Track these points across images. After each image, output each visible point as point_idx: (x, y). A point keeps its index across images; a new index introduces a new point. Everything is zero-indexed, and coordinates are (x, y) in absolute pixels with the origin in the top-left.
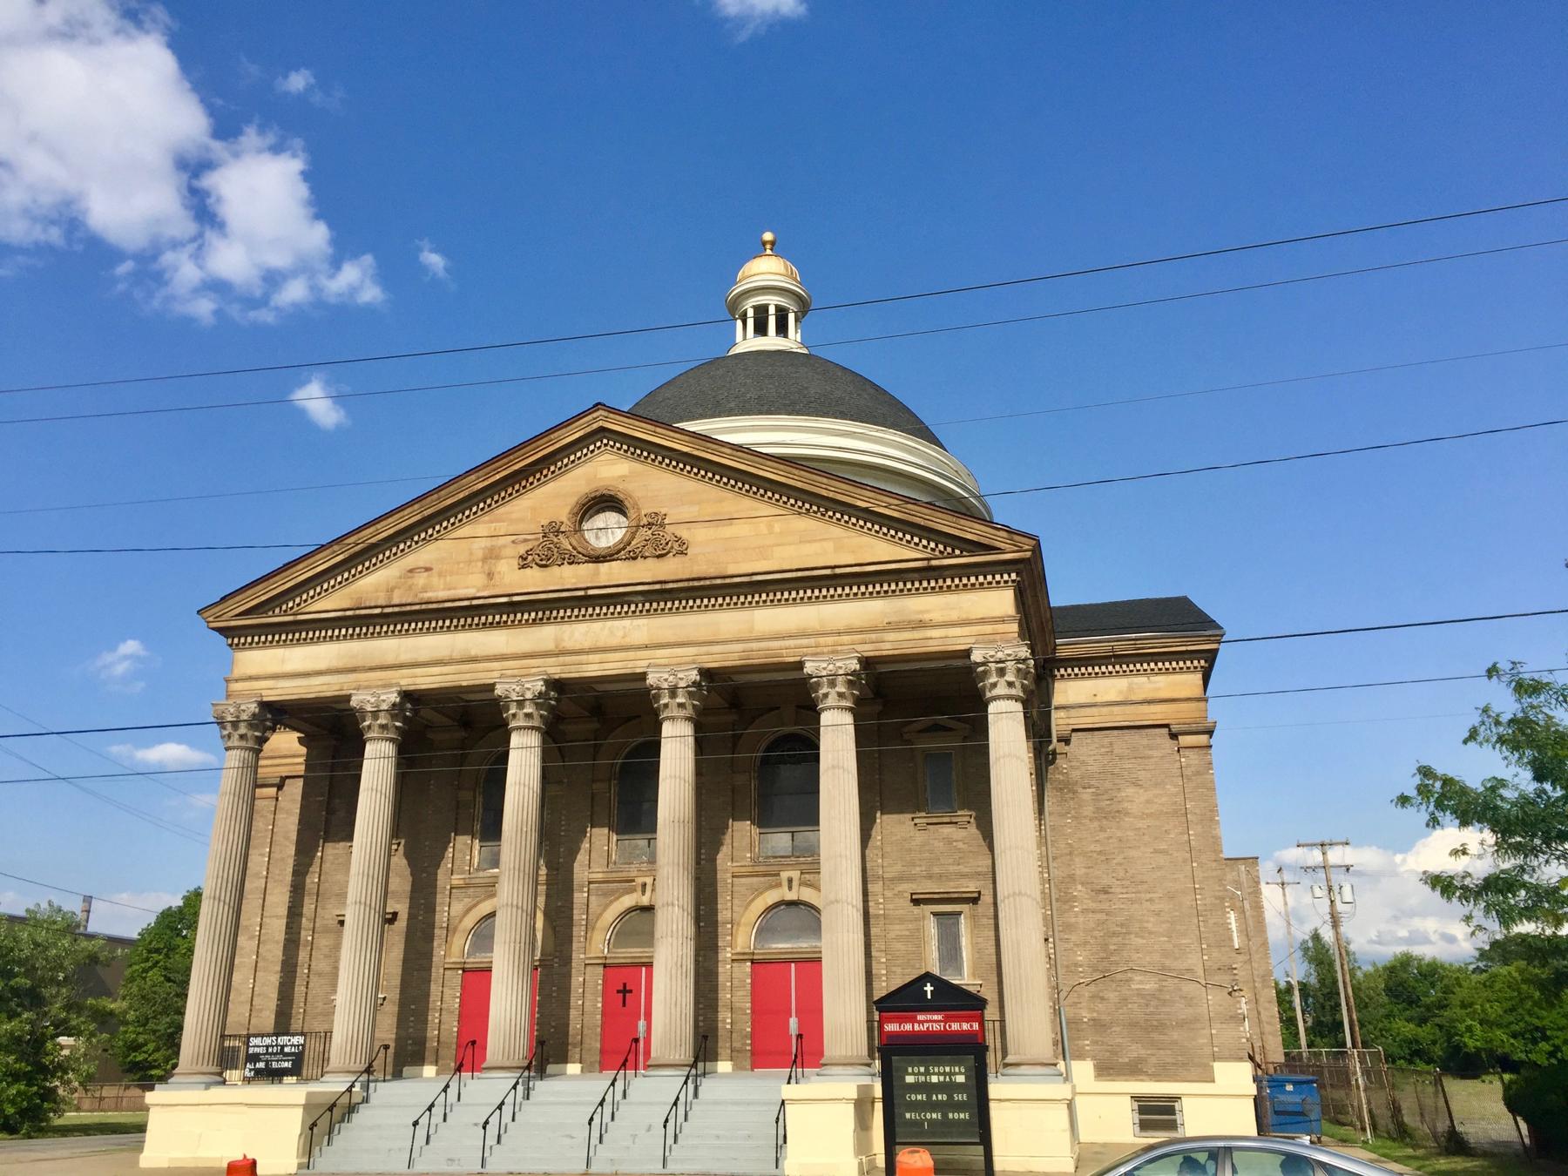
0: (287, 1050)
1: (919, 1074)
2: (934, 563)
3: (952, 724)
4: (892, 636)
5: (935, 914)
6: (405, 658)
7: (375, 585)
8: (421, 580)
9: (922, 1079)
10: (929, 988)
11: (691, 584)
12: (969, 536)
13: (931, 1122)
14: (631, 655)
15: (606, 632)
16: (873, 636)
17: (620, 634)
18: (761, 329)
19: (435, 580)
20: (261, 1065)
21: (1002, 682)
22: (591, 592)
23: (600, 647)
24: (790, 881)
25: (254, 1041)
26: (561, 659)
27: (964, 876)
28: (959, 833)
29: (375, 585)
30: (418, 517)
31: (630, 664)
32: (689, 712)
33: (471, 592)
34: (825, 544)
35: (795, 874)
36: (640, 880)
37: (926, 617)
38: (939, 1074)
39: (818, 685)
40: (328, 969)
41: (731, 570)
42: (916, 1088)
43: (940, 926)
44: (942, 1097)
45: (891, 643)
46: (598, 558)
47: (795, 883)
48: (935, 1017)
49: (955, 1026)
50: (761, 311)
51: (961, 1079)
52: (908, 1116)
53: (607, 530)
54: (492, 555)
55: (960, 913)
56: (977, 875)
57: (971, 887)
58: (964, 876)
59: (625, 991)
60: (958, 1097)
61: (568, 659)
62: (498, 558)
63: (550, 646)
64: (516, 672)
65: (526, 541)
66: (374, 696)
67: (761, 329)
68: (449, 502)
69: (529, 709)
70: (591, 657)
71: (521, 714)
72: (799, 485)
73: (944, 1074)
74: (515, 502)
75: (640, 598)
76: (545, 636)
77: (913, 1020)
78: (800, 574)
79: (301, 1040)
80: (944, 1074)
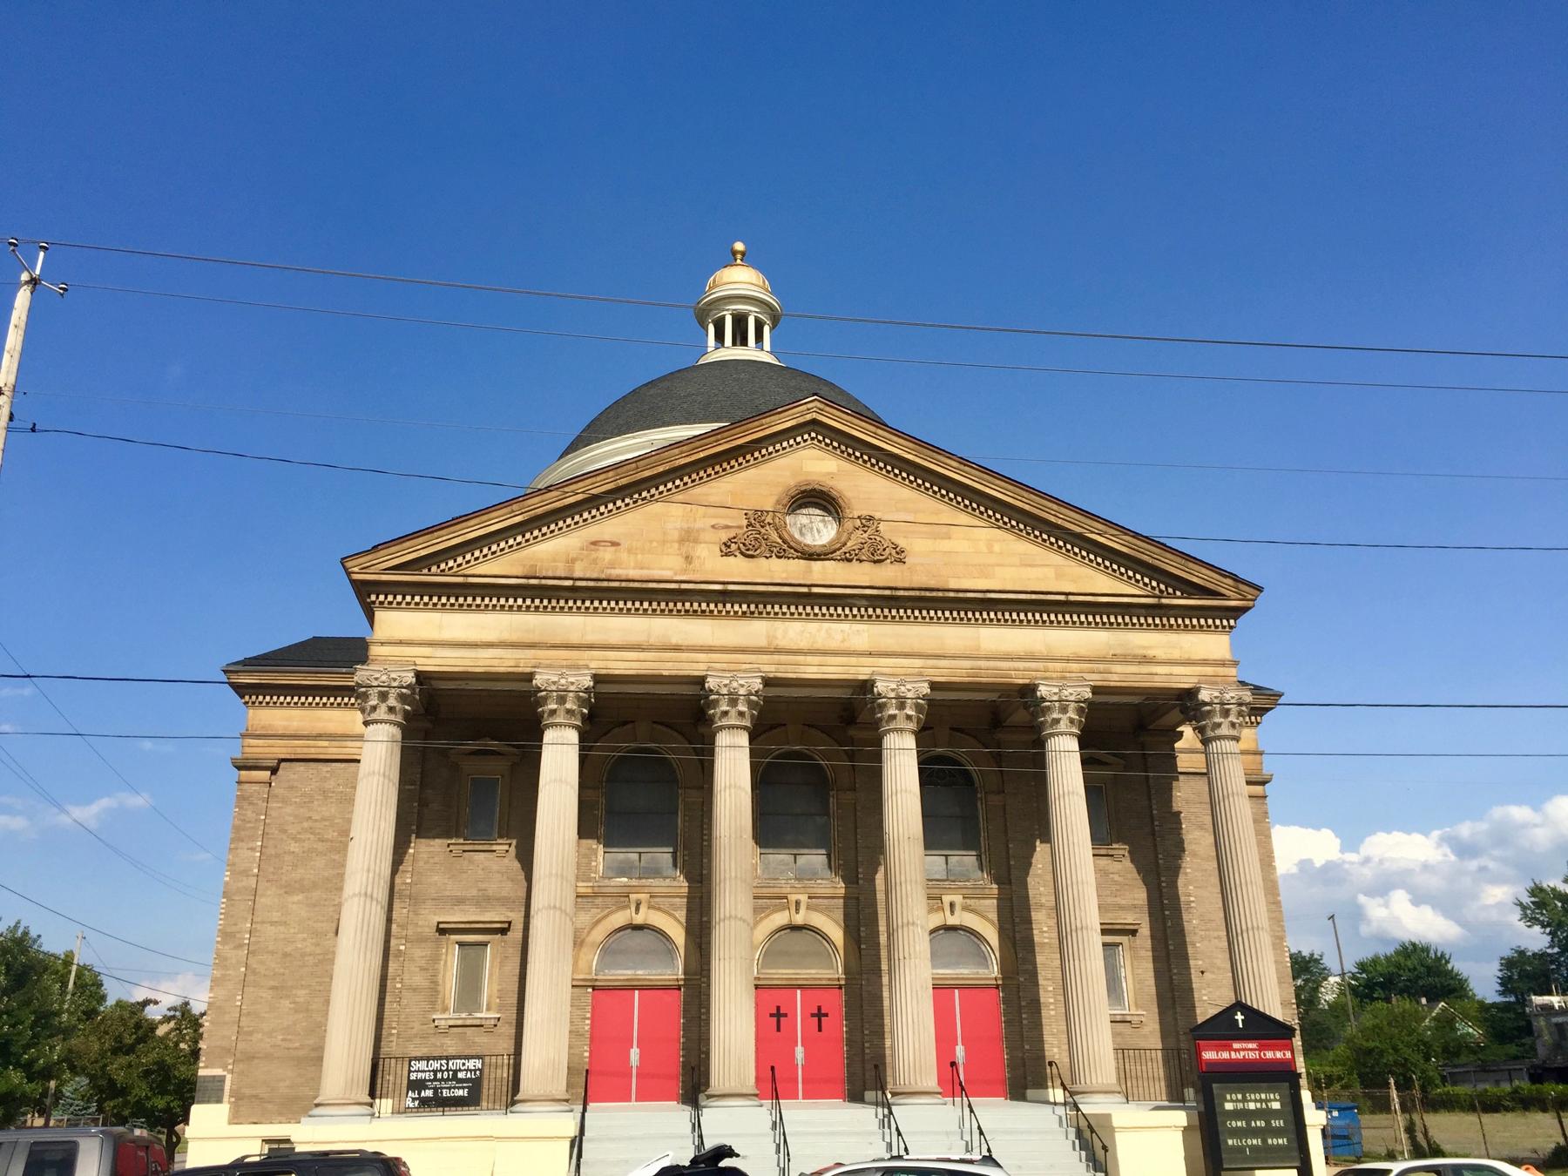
0: (460, 1075)
1: (1237, 1101)
2: (1164, 601)
3: (1111, 759)
4: (1118, 668)
5: (461, 944)
6: (614, 639)
7: (552, 553)
8: (607, 554)
9: (1240, 1106)
10: (1239, 1017)
11: (923, 593)
12: (1195, 580)
13: (1252, 1148)
14: (853, 660)
15: (823, 633)
16: (1101, 667)
17: (839, 637)
18: (720, 337)
19: (624, 556)
20: (429, 1093)
21: (383, 708)
22: (815, 590)
23: (826, 649)
24: (952, 905)
25: (416, 1065)
26: (776, 657)
27: (1122, 908)
28: (497, 860)
29: (552, 553)
30: (611, 486)
31: (853, 670)
32: (912, 726)
33: (667, 574)
34: (1046, 569)
35: (958, 899)
36: (793, 898)
37: (1151, 653)
38: (1256, 1101)
39: (545, 699)
40: (426, 984)
41: (953, 585)
42: (1237, 1114)
43: (462, 959)
44: (1261, 1124)
45: (1122, 675)
46: (811, 555)
47: (958, 908)
48: (1250, 1046)
49: (1269, 1055)
50: (740, 321)
51: (1276, 1105)
52: (1230, 1142)
53: (818, 530)
54: (688, 537)
55: (1117, 945)
56: (504, 901)
57: (494, 916)
58: (1122, 908)
59: (778, 1015)
60: (1276, 1123)
61: (783, 658)
62: (696, 541)
63: (763, 643)
64: (725, 666)
65: (727, 527)
66: (1063, 691)
67: (720, 337)
68: (647, 474)
69: (742, 708)
70: (809, 659)
71: (733, 712)
72: (1027, 507)
73: (1261, 1101)
74: (713, 484)
75: (865, 602)
76: (756, 631)
77: (1230, 1049)
78: (1034, 597)
79: (479, 1064)
80: (1261, 1101)
